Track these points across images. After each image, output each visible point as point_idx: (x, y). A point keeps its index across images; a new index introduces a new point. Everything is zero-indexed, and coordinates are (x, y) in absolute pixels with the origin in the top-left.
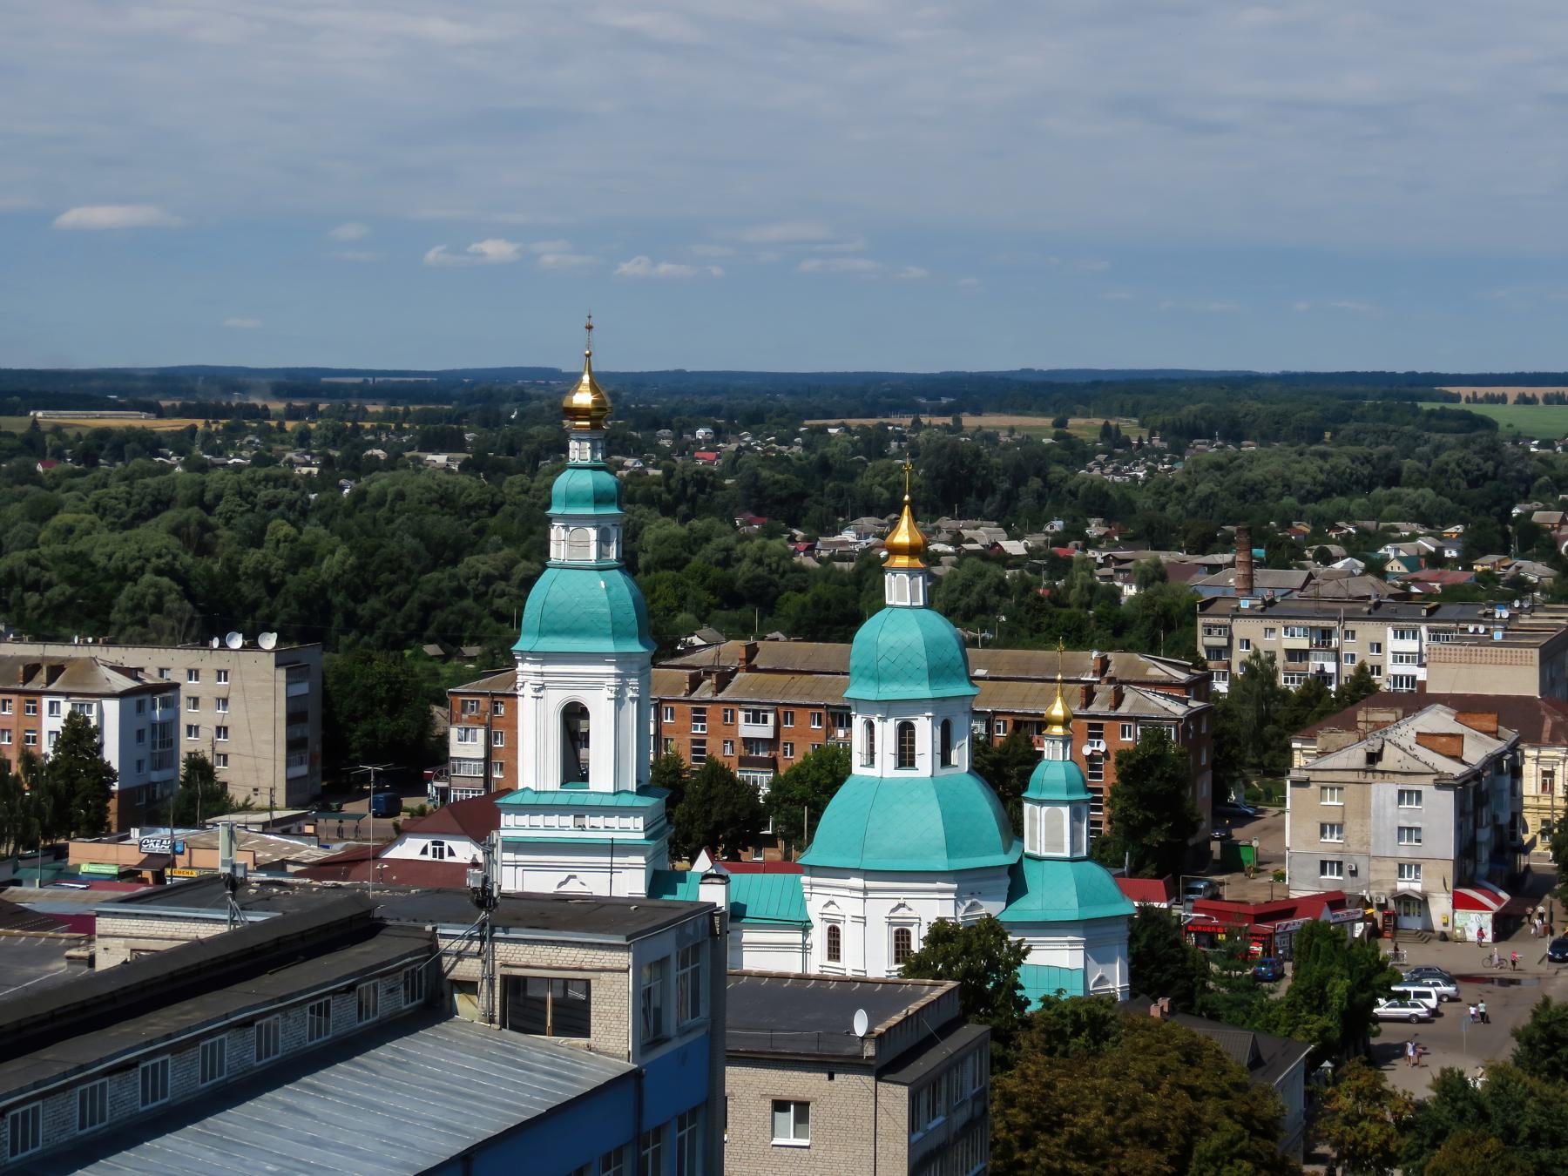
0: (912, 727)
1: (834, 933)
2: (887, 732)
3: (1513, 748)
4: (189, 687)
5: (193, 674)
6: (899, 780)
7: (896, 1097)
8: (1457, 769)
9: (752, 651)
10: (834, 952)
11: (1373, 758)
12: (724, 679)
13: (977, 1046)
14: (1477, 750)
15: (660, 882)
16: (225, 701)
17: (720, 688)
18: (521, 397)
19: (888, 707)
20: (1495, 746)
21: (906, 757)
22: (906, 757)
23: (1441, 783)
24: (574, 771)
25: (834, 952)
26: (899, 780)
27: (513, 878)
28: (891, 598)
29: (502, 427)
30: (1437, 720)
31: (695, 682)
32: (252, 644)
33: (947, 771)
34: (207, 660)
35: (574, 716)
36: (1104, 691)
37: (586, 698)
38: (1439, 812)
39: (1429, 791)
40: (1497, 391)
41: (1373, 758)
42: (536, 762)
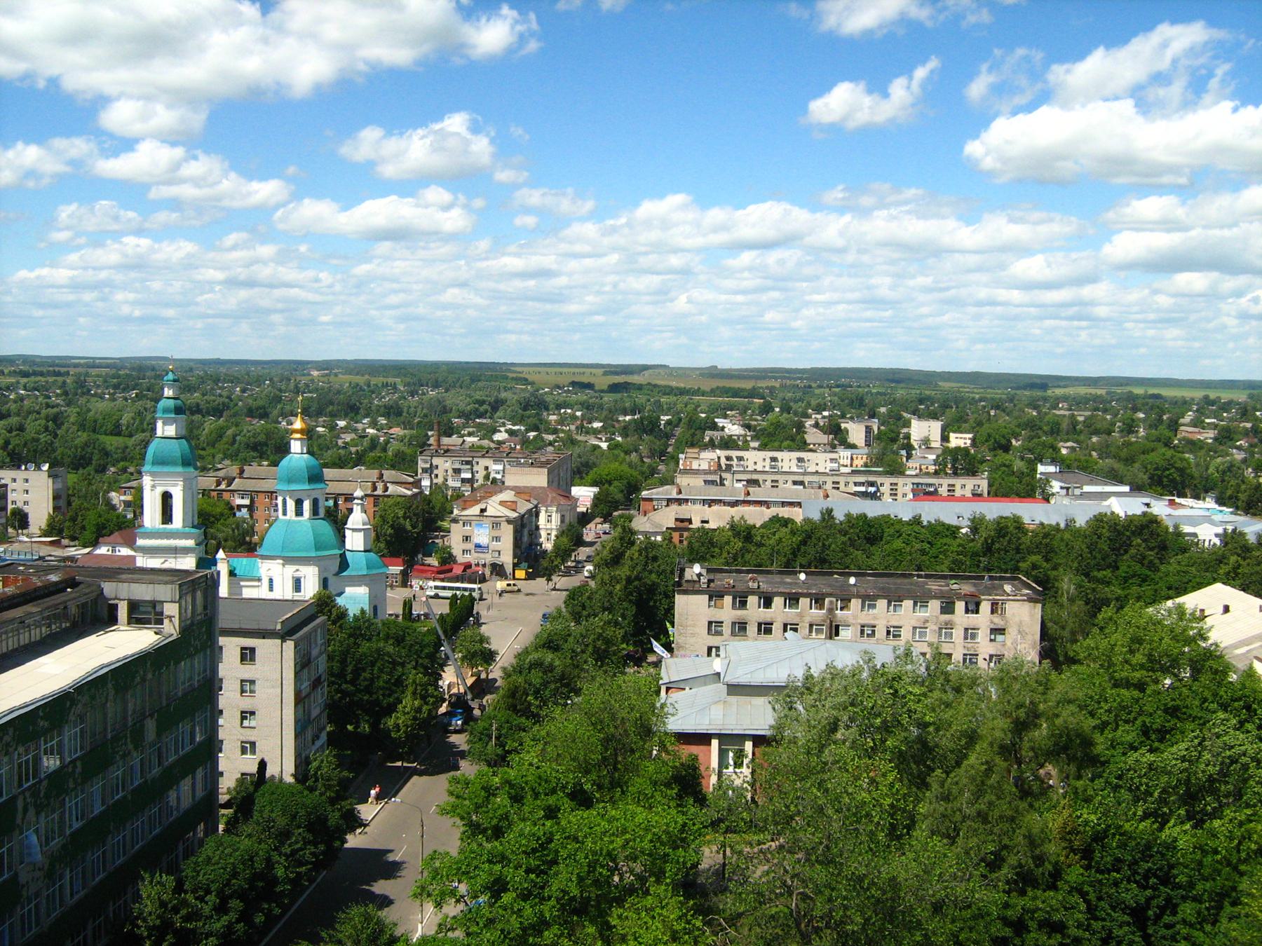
0: (171, 496)
1: (271, 581)
2: (291, 504)
3: (536, 507)
4: (11, 486)
5: (14, 480)
6: (291, 522)
7: (290, 645)
8: (515, 515)
9: (242, 471)
10: (271, 589)
11: (483, 511)
12: (230, 481)
13: (323, 625)
14: (524, 507)
15: (201, 563)
16: (27, 492)
17: (229, 485)
18: (153, 369)
19: (291, 493)
20: (531, 506)
21: (299, 512)
22: (299, 512)
23: (509, 522)
24: (167, 516)
25: (271, 589)
26: (291, 522)
27: (142, 562)
28: (292, 450)
29: (137, 379)
30: (508, 496)
31: (219, 484)
32: (38, 468)
33: (300, 518)
34: (20, 474)
35: (167, 497)
36: (380, 486)
37: (172, 490)
38: (507, 533)
39: (504, 525)
40: (582, 370)
41: (483, 511)
42: (151, 515)
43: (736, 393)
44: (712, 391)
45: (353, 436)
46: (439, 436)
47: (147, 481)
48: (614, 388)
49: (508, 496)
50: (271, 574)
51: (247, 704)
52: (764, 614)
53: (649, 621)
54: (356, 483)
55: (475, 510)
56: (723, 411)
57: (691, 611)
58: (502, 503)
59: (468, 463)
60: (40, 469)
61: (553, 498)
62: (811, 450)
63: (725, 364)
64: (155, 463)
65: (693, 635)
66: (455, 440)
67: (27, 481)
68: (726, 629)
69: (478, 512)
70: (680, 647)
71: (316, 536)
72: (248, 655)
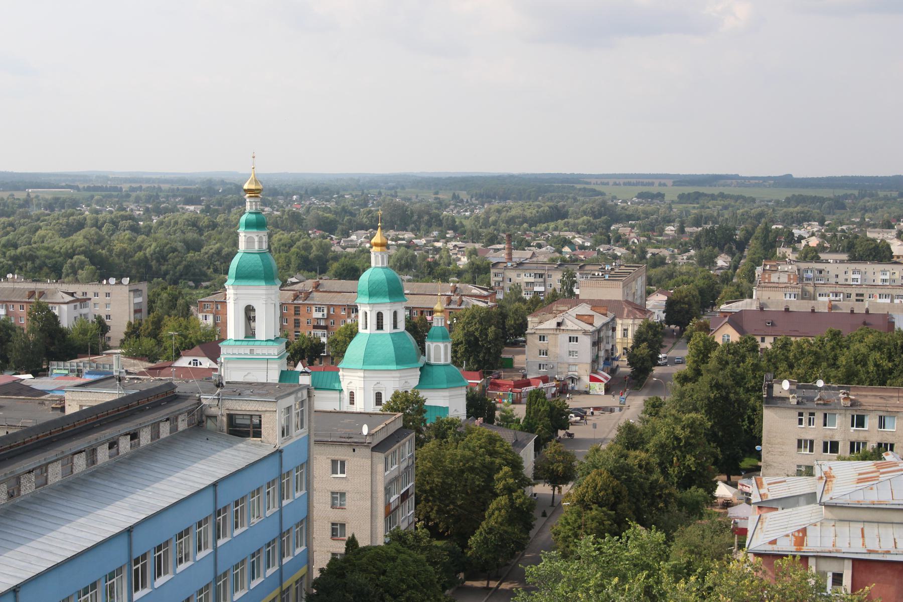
1: (352, 394)
5: (96, 294)
10: (352, 402)
12: (308, 295)
14: (599, 321)
23: (585, 333)
30: (584, 309)
38: (586, 342)
42: (234, 327)
43: (814, 200)
44: (788, 200)
45: (624, 250)
46: (510, 249)
47: (230, 293)
48: (683, 198)
49: (584, 309)
50: (352, 388)
51: (337, 516)
52: (854, 433)
53: (737, 448)
54: (435, 298)
55: (551, 324)
56: (801, 220)
57: (778, 427)
58: (579, 317)
59: (541, 276)
60: (120, 283)
61: (629, 311)
62: (896, 263)
63: (799, 173)
64: (240, 276)
65: (782, 453)
66: (527, 253)
67: (108, 295)
68: (818, 447)
69: (554, 326)
70: (768, 466)
71: (397, 348)
72: (338, 466)
